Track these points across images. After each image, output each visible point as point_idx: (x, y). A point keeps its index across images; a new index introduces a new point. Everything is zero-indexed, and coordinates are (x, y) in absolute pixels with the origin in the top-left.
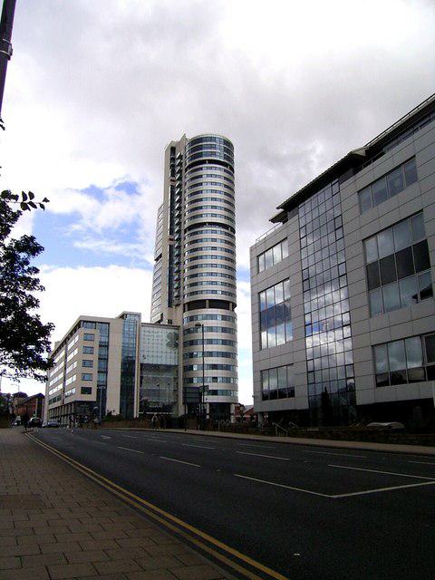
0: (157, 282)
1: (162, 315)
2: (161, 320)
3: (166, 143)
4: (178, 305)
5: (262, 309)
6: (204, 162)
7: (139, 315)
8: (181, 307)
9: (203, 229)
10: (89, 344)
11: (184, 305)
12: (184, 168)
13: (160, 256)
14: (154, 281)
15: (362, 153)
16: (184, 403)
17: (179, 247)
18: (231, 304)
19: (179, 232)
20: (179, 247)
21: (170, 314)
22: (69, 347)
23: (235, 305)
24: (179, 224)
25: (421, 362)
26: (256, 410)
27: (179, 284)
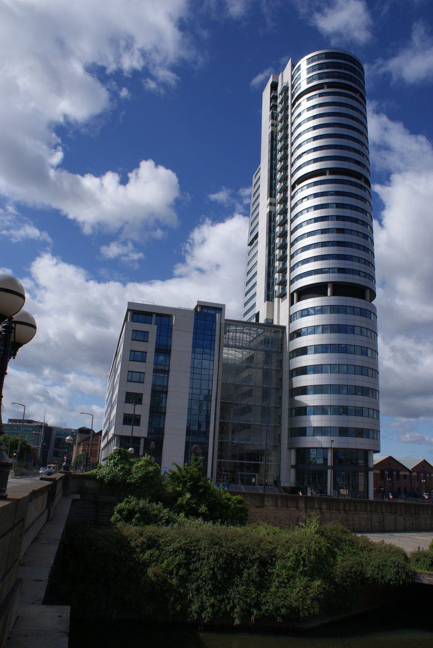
4: (282, 296)
8: (287, 300)
10: (140, 346)
11: (292, 295)
16: (290, 449)
18: (368, 293)
21: (270, 310)
23: (373, 295)
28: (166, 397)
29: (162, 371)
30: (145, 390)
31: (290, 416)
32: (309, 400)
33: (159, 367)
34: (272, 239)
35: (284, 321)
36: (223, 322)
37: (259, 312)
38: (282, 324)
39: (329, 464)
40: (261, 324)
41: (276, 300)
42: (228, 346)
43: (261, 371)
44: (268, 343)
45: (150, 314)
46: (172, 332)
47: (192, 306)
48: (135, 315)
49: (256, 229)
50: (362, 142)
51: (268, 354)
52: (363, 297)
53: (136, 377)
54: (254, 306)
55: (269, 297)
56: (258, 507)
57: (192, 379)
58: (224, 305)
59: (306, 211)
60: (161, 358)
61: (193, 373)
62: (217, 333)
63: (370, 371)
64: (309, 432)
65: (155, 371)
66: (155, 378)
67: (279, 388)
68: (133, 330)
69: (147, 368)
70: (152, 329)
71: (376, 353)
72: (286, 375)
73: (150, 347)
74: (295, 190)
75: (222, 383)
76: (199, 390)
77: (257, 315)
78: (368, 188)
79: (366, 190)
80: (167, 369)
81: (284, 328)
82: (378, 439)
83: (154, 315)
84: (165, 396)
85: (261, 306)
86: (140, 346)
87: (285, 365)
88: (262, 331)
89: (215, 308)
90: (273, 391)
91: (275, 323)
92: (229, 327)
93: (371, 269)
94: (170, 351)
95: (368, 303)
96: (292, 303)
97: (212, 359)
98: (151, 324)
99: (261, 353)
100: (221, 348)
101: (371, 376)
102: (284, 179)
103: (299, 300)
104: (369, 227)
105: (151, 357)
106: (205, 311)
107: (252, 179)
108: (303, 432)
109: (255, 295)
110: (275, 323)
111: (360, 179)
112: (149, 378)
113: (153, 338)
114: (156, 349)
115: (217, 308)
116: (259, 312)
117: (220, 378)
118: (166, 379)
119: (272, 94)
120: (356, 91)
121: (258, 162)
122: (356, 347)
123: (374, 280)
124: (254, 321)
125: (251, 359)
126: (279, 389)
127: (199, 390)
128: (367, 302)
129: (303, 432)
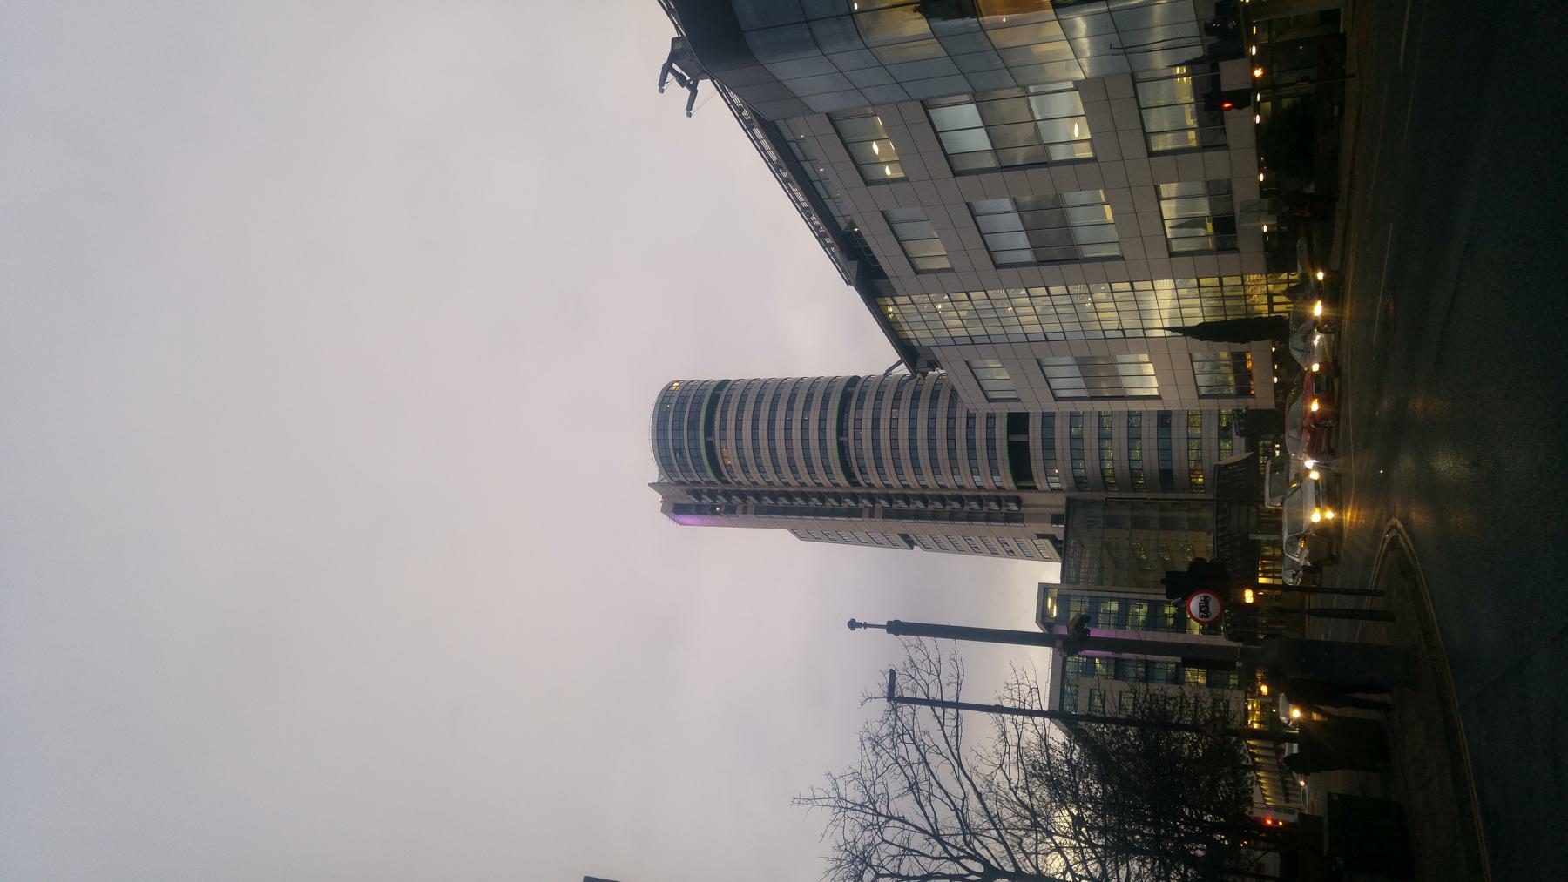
0: (1013, 546)
1: (1040, 536)
2: (1053, 539)
3: (666, 523)
4: (1018, 501)
5: (1084, 393)
6: (710, 447)
7: (1045, 590)
8: (1024, 495)
9: (851, 447)
11: (1020, 488)
12: (720, 487)
13: (905, 537)
14: (943, 549)
15: (854, 266)
17: (889, 498)
19: (855, 498)
20: (889, 498)
21: (1038, 518)
22: (966, 872)
24: (838, 497)
25: (1105, 207)
26: (1305, 481)
35: (1061, 500)
58: (1040, 585)
74: (730, 480)
81: (1069, 500)
91: (1063, 511)
93: (735, 391)
96: (1034, 488)
103: (1031, 478)
111: (718, 397)
129: (1166, 476)
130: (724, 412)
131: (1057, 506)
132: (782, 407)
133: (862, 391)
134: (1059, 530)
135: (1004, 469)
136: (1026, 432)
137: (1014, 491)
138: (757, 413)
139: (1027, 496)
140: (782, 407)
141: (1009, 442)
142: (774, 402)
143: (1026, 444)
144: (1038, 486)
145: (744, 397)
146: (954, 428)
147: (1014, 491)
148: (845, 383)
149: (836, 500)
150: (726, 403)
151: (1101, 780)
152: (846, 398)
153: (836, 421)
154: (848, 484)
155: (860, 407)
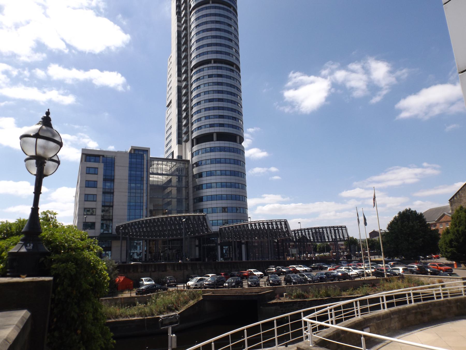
4: (187, 141)
10: (92, 178)
11: (193, 140)
19: (186, 72)
23: (242, 140)
24: (187, 133)
27: (188, 121)
28: (113, 209)
29: (108, 192)
30: (98, 206)
31: (194, 203)
32: (205, 180)
33: (107, 190)
34: (180, 97)
36: (149, 159)
37: (173, 151)
38: (188, 159)
39: (219, 247)
40: (175, 160)
41: (183, 143)
42: (153, 174)
43: (175, 188)
44: (179, 170)
45: (99, 156)
46: (114, 167)
47: (129, 151)
48: (87, 157)
49: (170, 116)
50: (230, 18)
51: (180, 180)
52: (235, 141)
53: (92, 171)
54: (171, 147)
55: (179, 142)
56: (163, 271)
57: (130, 196)
58: (149, 148)
59: (199, 56)
60: (108, 184)
61: (130, 193)
62: (145, 166)
63: (240, 173)
64: (205, 198)
65: (104, 193)
66: (105, 185)
67: (187, 176)
68: (86, 181)
69: (98, 192)
70: (100, 166)
71: (244, 174)
72: (190, 179)
73: (99, 178)
75: (150, 198)
76: (134, 207)
77: (173, 153)
78: (239, 73)
79: (232, 34)
80: (112, 191)
81: (189, 161)
82: (246, 213)
83: (101, 157)
84: (112, 209)
85: (175, 148)
86: (92, 178)
87: (190, 172)
88: (175, 163)
89: (143, 150)
90: (184, 200)
91: (184, 158)
92: (153, 162)
93: (236, 83)
94: (114, 179)
95: (239, 145)
97: (142, 205)
98: (99, 162)
99: (176, 177)
100: (148, 176)
101: (241, 188)
102: (186, 64)
103: (197, 143)
104: (239, 97)
105: (100, 184)
106: (137, 152)
107: (167, 81)
108: (201, 199)
109: (171, 140)
110: (184, 158)
111: (233, 66)
112: (100, 198)
113: (101, 171)
114: (103, 179)
115: (145, 150)
116: (173, 151)
117: (149, 194)
118: (112, 197)
119: (177, 4)
120: (230, 6)
121: (170, 52)
122: (231, 160)
123: (242, 130)
124: (171, 157)
125: (170, 181)
126: (187, 187)
127: (134, 194)
128: (231, 57)
129: (201, 199)
130: (224, 9)
131: (185, 157)
132: (231, 122)
133: (236, 111)
134: (175, 157)
135: (200, 83)
136: (217, 140)
137: (191, 138)
138: (223, 23)
139: (189, 144)
140: (231, 122)
141: (213, 133)
142: (232, 102)
143: (212, 140)
144: (194, 147)
145: (234, 95)
146: (219, 110)
147: (191, 138)
148: (241, 135)
149: (185, 108)
150: (228, 11)
151: (69, 240)
152: (232, 64)
153: (225, 142)
154: (193, 137)
155: (227, 69)
